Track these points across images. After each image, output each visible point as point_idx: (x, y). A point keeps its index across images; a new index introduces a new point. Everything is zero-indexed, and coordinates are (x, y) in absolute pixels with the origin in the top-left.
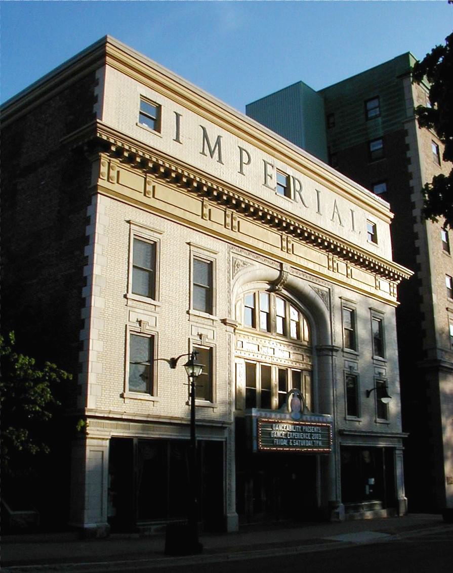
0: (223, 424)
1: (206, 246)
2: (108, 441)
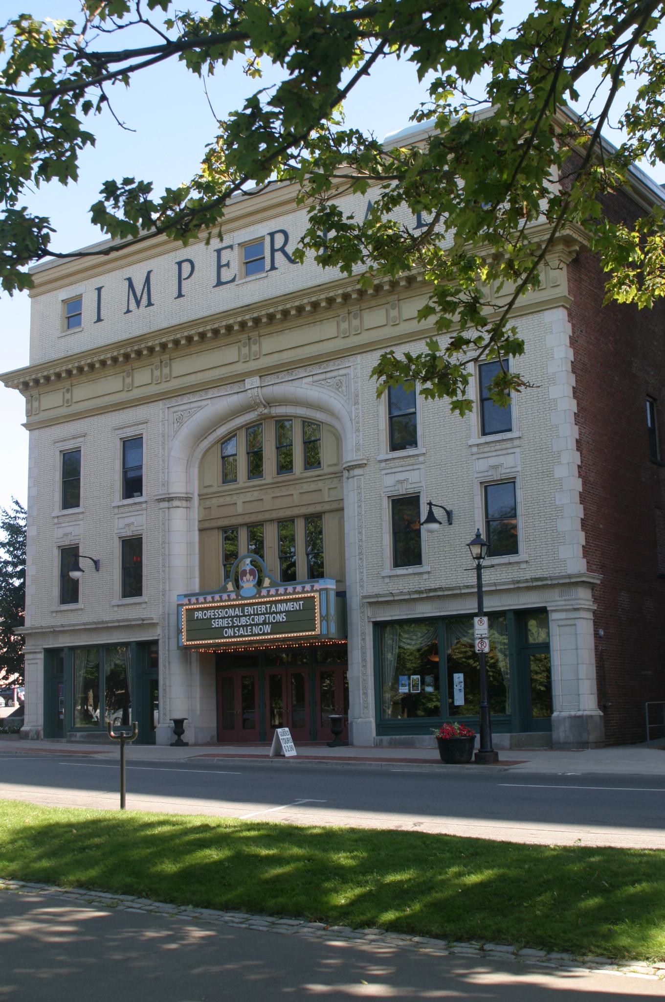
0: (143, 620)
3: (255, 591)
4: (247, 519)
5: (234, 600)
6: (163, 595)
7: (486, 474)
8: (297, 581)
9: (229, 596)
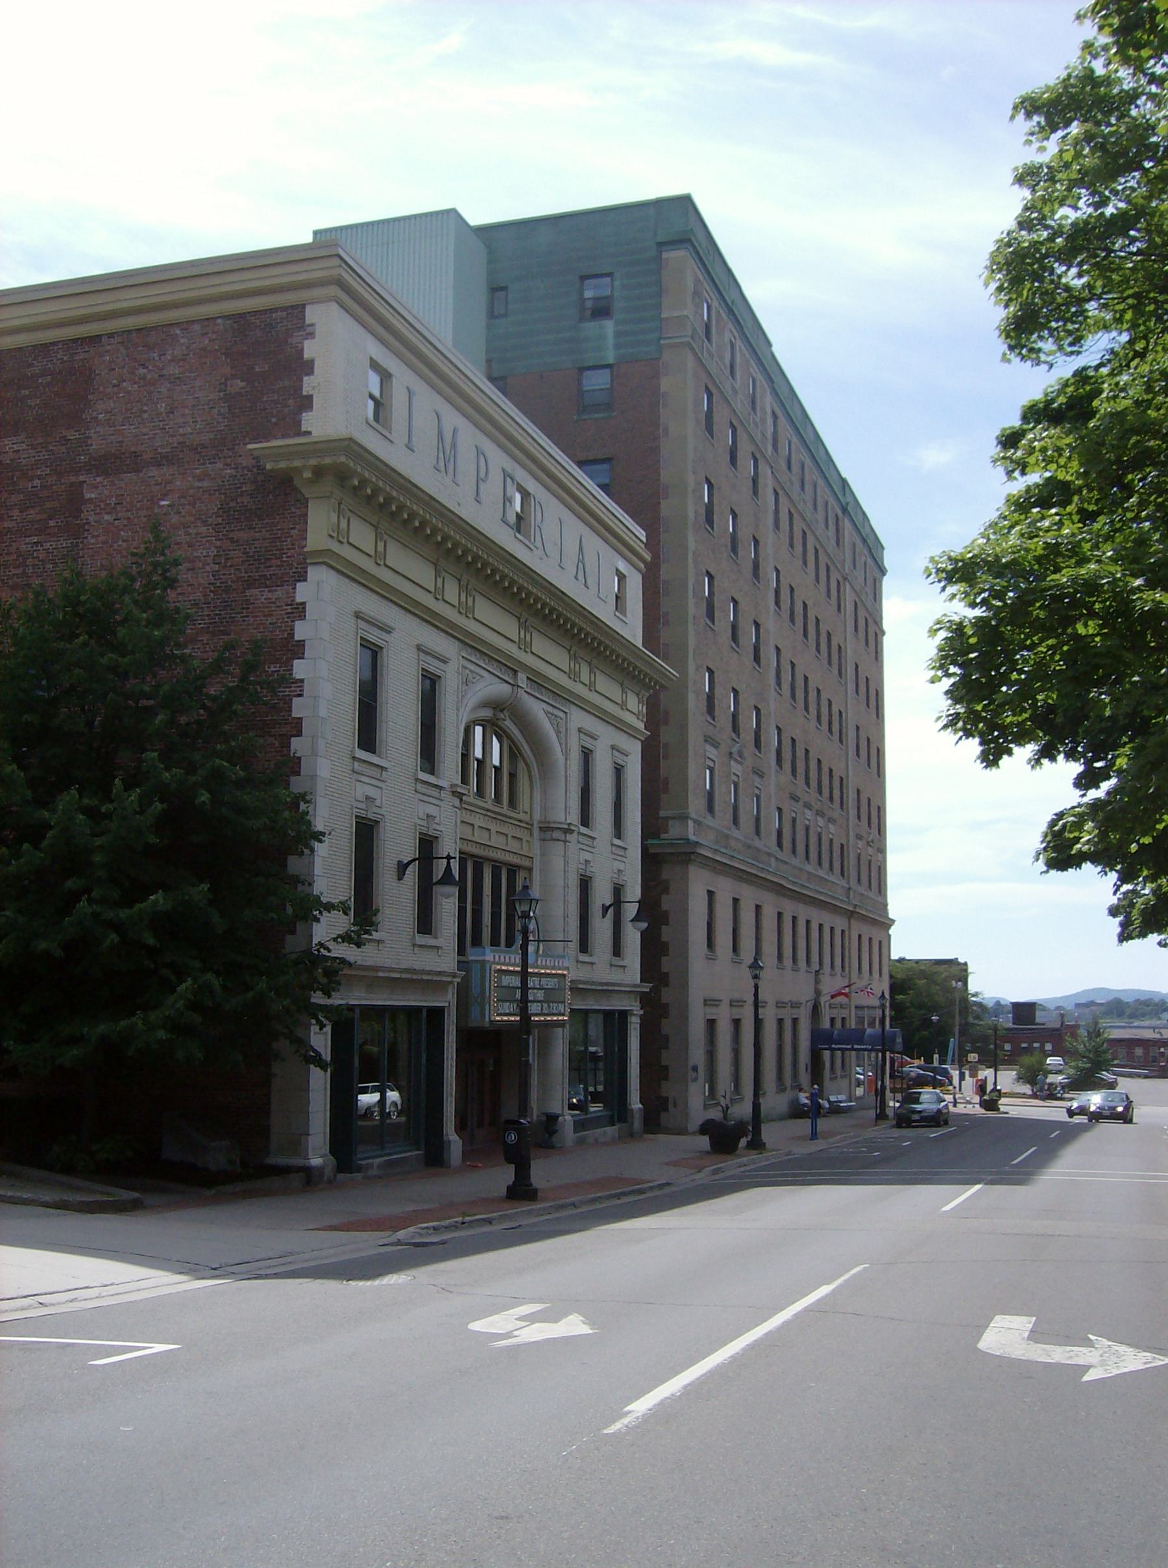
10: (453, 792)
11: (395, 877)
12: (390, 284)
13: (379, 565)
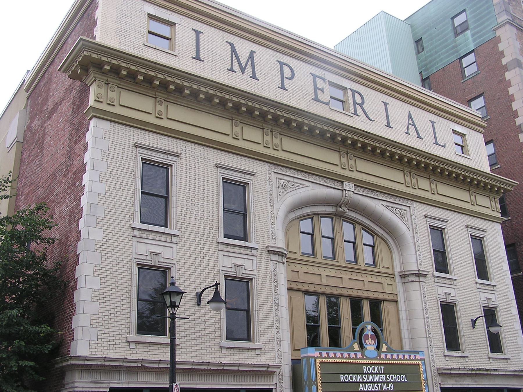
0: (268, 367)
1: (239, 167)
2: (108, 389)
3: (376, 353)
4: (329, 291)
5: (360, 359)
6: (278, 344)
7: (144, 257)
8: (322, 347)
9: (356, 355)
10: (268, 251)
11: (472, 327)
12: (342, 52)
13: (474, 205)
